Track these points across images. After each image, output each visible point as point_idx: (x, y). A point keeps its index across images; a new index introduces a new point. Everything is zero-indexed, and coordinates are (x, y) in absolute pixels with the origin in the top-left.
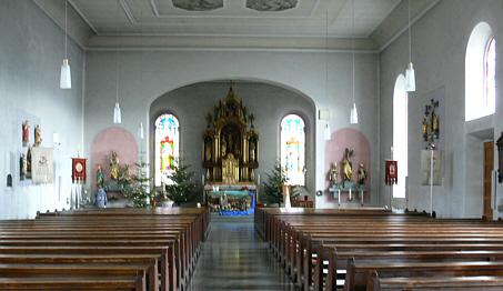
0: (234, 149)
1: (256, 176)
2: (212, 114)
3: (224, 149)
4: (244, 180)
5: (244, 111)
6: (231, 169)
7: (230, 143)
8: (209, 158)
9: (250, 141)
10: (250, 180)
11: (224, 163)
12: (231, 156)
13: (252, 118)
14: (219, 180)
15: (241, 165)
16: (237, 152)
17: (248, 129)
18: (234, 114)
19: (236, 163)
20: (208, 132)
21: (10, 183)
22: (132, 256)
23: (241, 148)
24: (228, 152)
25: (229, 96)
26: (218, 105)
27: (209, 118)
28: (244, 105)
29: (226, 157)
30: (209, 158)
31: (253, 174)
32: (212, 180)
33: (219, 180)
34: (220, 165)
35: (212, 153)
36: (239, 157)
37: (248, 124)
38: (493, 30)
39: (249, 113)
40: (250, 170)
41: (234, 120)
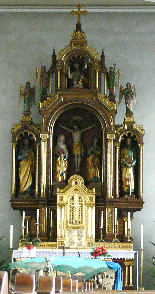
0: (85, 164)
1: (136, 228)
2: (36, 84)
3: (63, 167)
4: (108, 238)
5: (110, 77)
6: (76, 206)
7: (77, 151)
8: (26, 185)
9: (123, 145)
10: (122, 238)
11: (64, 197)
12: (77, 181)
13: (127, 93)
14: (50, 236)
15: (101, 203)
16: (93, 171)
17: (119, 119)
18: (86, 86)
19: (90, 197)
20: (25, 125)
21: (77, 242)
22: (37, 165)
23: (100, 163)
24: (70, 172)
25: (73, 42)
26: (48, 64)
27: (28, 94)
28: (108, 64)
29: (65, 184)
30: (26, 185)
31: (130, 225)
32: (30, 238)
33: (50, 236)
34: (51, 203)
35: (34, 173)
36: (94, 183)
37: (121, 108)
38: (134, 165)
39: (121, 82)
40: (121, 216)
41: (86, 97)
